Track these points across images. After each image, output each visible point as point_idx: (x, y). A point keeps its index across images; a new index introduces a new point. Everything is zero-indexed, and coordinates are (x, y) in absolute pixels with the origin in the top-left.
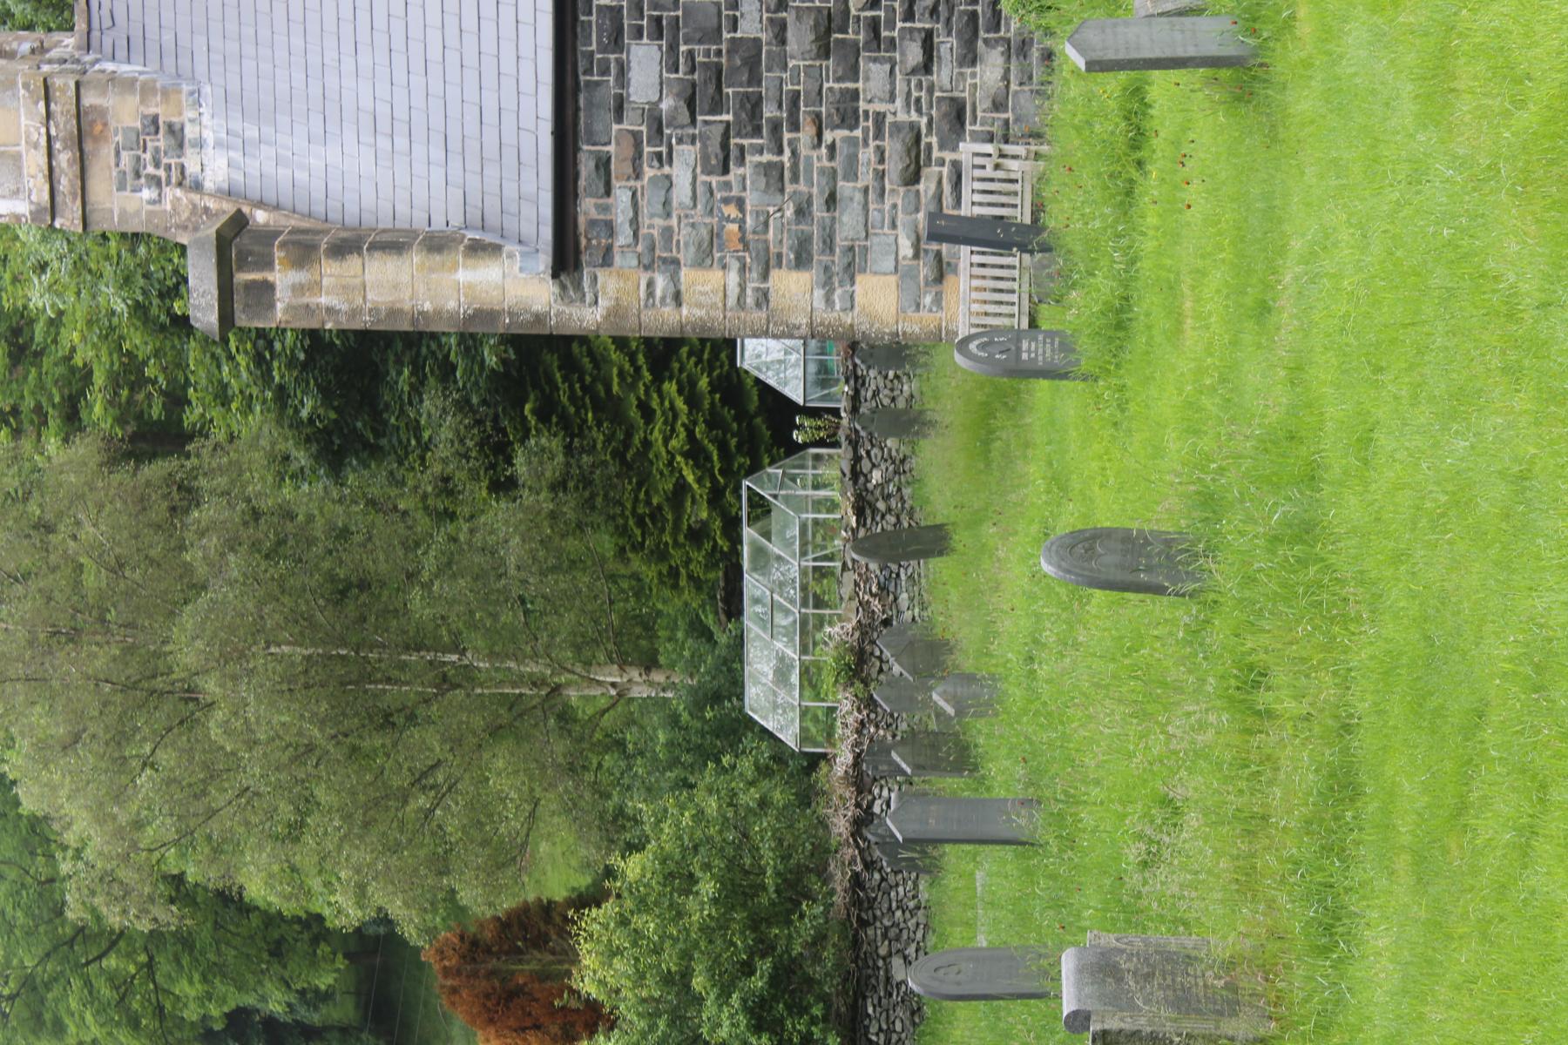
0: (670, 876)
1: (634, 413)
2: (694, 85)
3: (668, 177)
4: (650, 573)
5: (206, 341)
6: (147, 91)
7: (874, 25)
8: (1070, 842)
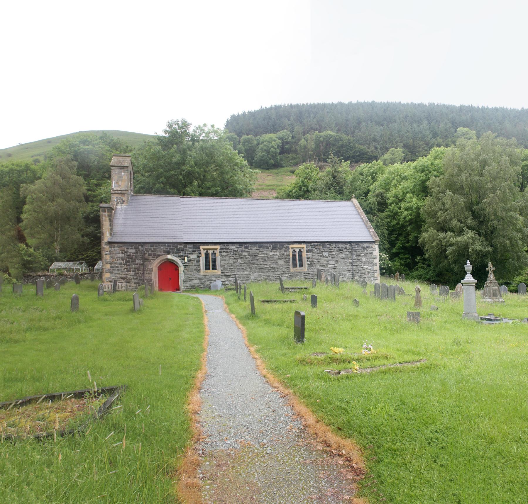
0: (31, 254)
1: (92, 250)
4: (72, 251)
5: (99, 205)
6: (127, 201)
7: (138, 273)
8: (37, 300)
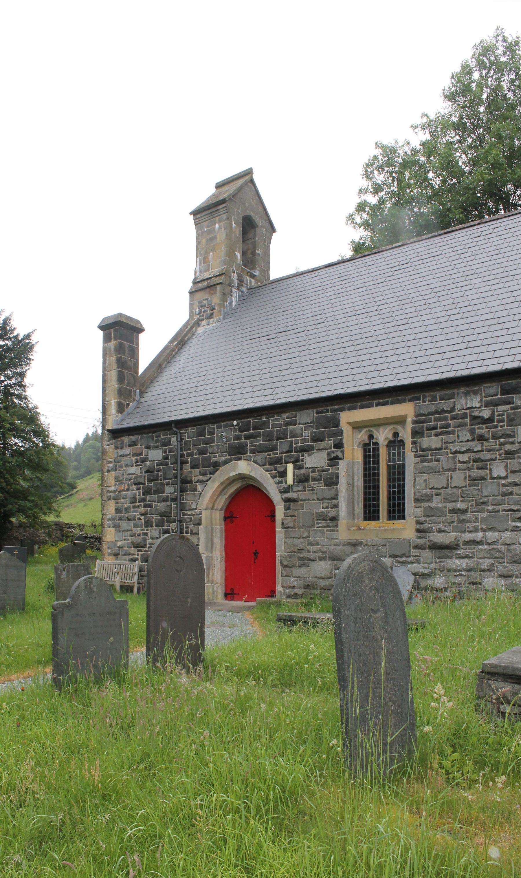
2: (152, 472)
3: (132, 466)
